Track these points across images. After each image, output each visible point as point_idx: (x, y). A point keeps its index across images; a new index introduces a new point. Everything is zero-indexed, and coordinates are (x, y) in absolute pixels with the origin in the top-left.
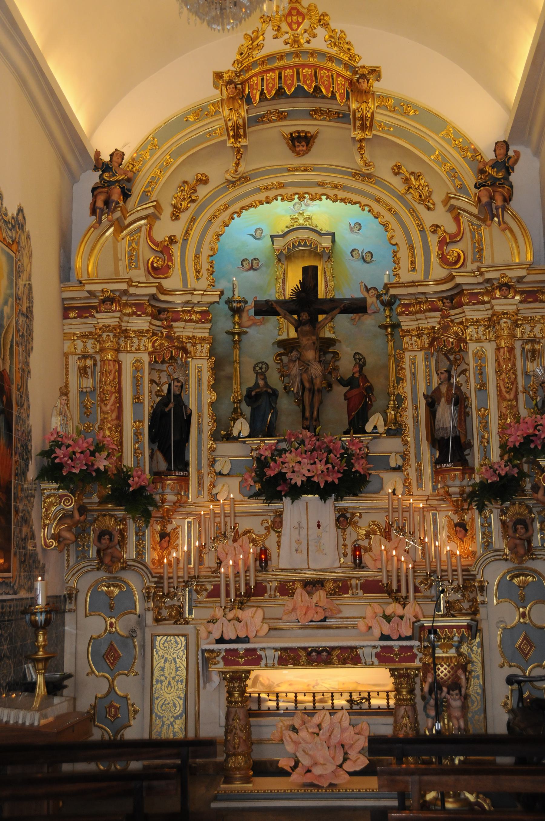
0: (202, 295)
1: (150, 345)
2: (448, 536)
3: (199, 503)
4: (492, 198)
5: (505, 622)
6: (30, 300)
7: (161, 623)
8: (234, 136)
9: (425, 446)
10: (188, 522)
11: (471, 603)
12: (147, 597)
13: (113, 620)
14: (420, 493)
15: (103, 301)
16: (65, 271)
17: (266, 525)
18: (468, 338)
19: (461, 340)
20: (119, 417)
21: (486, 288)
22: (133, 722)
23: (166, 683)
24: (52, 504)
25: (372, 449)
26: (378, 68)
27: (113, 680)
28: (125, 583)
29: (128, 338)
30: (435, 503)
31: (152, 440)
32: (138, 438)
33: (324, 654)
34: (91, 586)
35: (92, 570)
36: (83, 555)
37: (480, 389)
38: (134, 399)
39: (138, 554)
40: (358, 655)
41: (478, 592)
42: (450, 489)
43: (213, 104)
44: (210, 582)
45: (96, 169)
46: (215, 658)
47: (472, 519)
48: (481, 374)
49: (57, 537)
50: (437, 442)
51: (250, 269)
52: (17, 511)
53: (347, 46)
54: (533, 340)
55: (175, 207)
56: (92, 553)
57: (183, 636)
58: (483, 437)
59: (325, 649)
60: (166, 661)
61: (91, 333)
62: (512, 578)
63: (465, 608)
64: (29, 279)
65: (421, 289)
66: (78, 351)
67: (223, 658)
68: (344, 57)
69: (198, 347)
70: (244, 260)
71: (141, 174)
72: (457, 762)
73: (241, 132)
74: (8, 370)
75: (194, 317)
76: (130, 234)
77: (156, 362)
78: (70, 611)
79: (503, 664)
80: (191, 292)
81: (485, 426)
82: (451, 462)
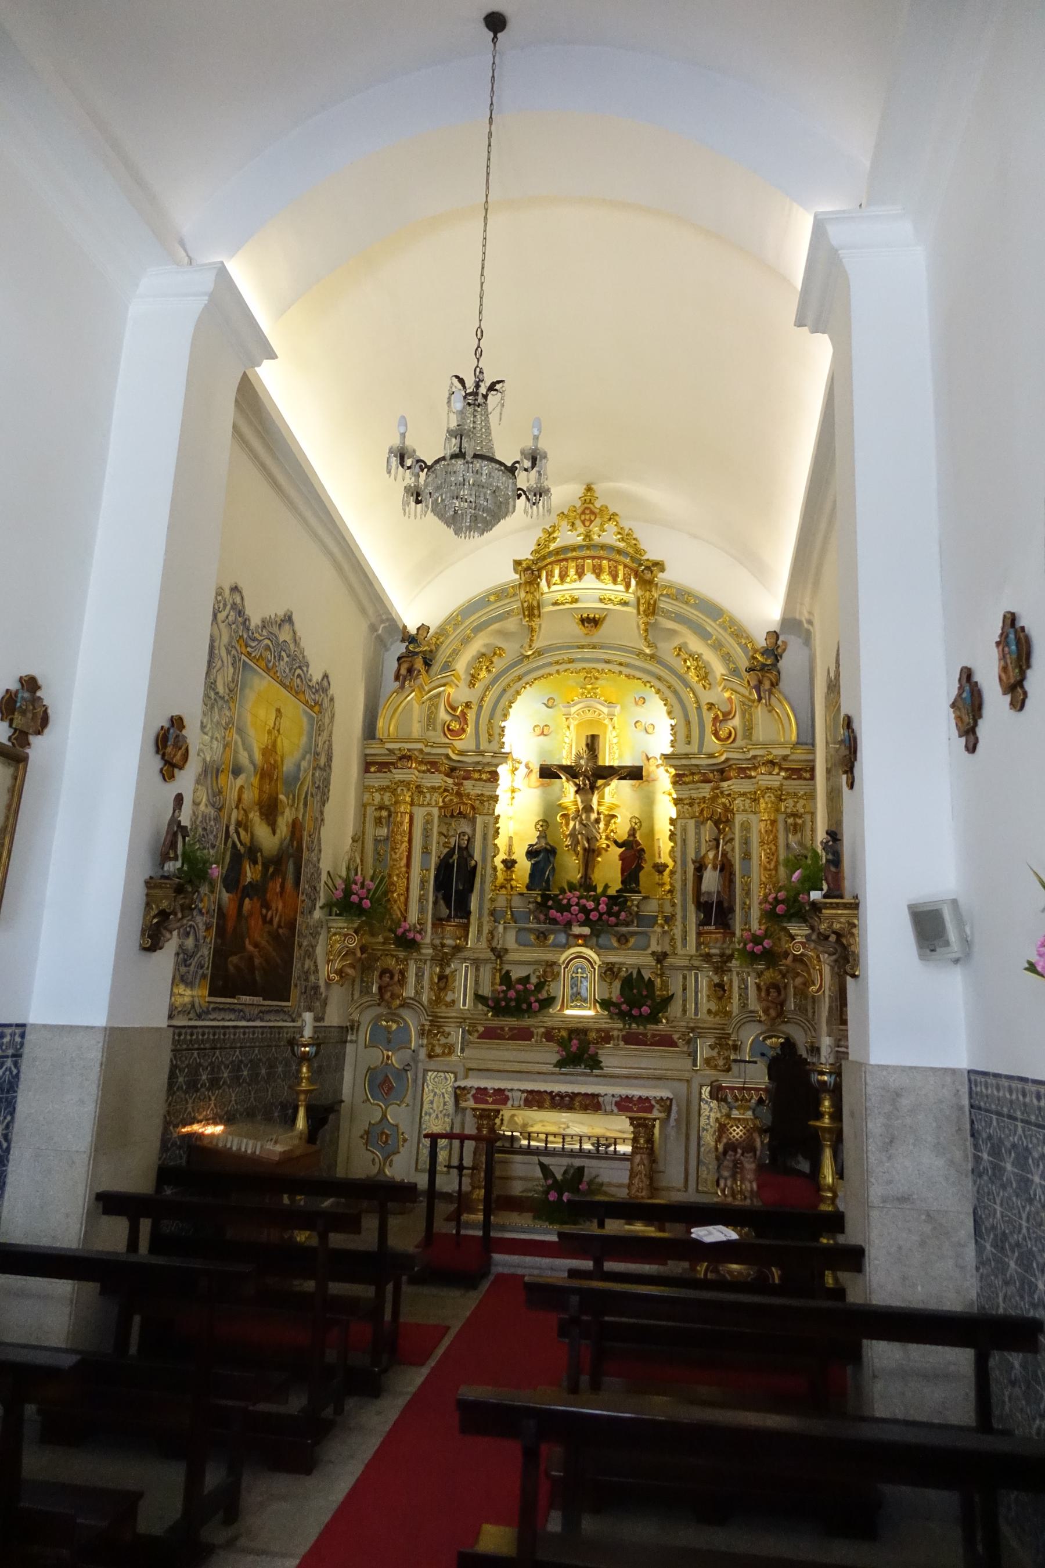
4: (760, 682)
6: (330, 759)
8: (529, 616)
9: (691, 908)
12: (422, 1033)
13: (390, 1053)
15: (400, 759)
16: (370, 732)
19: (727, 809)
20: (408, 865)
22: (401, 1149)
23: (434, 1115)
24: (336, 941)
25: (642, 908)
27: (387, 1108)
28: (404, 1020)
29: (421, 792)
31: (437, 888)
36: (366, 991)
37: (744, 858)
39: (417, 992)
40: (598, 1102)
43: (513, 587)
45: (403, 641)
47: (731, 981)
48: (746, 843)
49: (340, 972)
50: (703, 906)
52: (300, 946)
54: (795, 815)
55: (473, 676)
56: (375, 989)
58: (745, 903)
59: (567, 1095)
60: (435, 1094)
61: (388, 787)
64: (330, 736)
65: (694, 762)
66: (376, 802)
67: (473, 1096)
68: (630, 550)
69: (486, 804)
71: (444, 646)
72: (565, 1199)
73: (536, 612)
74: (300, 817)
75: (484, 776)
76: (430, 699)
78: (351, 1042)
80: (481, 753)
81: (748, 893)
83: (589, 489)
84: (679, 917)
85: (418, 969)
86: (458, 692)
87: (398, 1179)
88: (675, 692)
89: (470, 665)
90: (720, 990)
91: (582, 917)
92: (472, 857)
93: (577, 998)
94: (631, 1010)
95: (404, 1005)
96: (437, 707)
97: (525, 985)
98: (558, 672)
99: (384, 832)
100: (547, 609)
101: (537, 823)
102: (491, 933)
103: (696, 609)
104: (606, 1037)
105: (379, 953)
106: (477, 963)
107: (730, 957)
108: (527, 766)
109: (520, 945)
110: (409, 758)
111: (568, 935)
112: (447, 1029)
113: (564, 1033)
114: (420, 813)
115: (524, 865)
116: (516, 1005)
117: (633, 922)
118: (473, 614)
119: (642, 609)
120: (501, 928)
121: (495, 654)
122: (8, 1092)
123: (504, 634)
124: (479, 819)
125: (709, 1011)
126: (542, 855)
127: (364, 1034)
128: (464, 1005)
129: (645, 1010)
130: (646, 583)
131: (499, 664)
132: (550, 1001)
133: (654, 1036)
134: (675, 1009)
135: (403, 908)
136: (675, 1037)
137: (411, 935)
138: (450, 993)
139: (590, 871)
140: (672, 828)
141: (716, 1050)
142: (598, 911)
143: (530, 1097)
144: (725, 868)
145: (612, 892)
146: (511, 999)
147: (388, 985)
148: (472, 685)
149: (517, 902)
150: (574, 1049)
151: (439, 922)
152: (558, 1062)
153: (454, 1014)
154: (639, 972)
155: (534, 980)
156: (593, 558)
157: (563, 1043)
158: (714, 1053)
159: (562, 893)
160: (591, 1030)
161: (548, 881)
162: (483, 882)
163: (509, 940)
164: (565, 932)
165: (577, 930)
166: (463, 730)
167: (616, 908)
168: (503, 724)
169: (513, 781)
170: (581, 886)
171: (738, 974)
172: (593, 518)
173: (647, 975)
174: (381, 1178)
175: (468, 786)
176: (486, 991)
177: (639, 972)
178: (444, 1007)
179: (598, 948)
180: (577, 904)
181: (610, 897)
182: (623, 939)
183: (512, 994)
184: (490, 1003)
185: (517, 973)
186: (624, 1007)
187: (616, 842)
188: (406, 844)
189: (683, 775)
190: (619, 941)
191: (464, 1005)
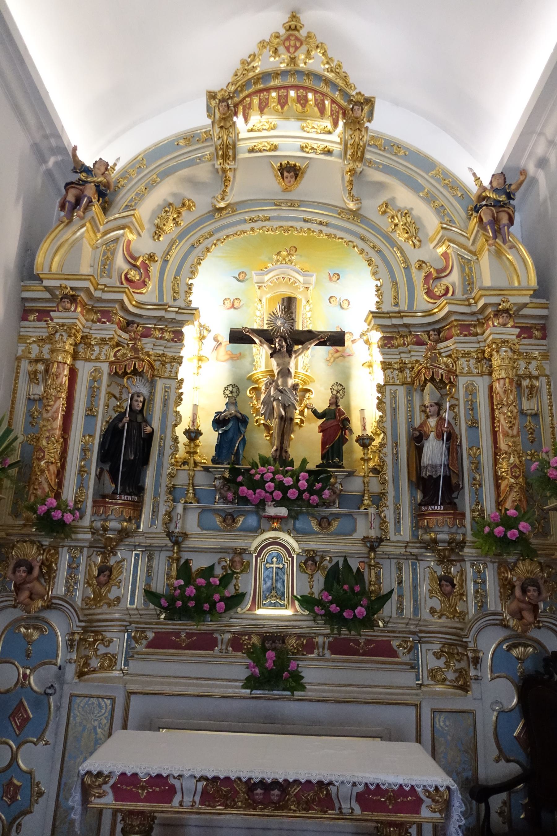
0: (177, 312)
1: (112, 354)
2: (430, 590)
3: (151, 533)
5: (501, 703)
7: (86, 677)
11: (457, 675)
12: (70, 645)
17: (224, 564)
18: (458, 371)
21: (478, 320)
26: (374, 98)
27: (18, 748)
29: (89, 345)
30: (415, 551)
32: (86, 455)
37: (471, 427)
38: (86, 411)
39: (68, 590)
40: (329, 794)
41: (471, 665)
42: (438, 536)
46: (100, 786)
47: (462, 573)
48: (472, 409)
51: (231, 308)
53: (344, 74)
55: (158, 227)
58: (474, 479)
63: (449, 678)
65: (407, 321)
67: (113, 787)
68: (341, 84)
69: (168, 366)
70: (225, 299)
77: (116, 373)
79: (499, 757)
80: (163, 306)
82: (441, 504)
83: (294, 17)
84: (390, 496)
85: (73, 559)
86: (143, 245)
88: (379, 252)
89: (155, 214)
90: (446, 585)
91: (278, 494)
92: (147, 422)
93: (276, 595)
94: (342, 611)
95: (50, 606)
96: (113, 253)
97: (207, 579)
98: (253, 229)
99: (39, 390)
100: (243, 155)
101: (226, 389)
102: (169, 514)
103: (406, 160)
104: (309, 646)
105: (15, 539)
106: (150, 551)
107: (462, 544)
108: (216, 339)
109: (203, 529)
110: (73, 299)
111: (260, 518)
112: (108, 635)
113: (255, 640)
114: (85, 370)
115: (210, 438)
116: (196, 604)
117: (334, 502)
118: (159, 160)
119: (349, 152)
120: (180, 508)
121: (184, 205)
123: (193, 182)
124: (160, 384)
125: (433, 611)
126: (231, 425)
128: (132, 603)
129: (361, 611)
130: (355, 124)
131: (187, 218)
133: (368, 642)
134: (390, 609)
135: (53, 481)
136: (395, 643)
137: (58, 515)
138: (114, 588)
139: (286, 443)
140: (379, 395)
141: (443, 660)
142: (298, 488)
144: (450, 438)
145: (311, 466)
146: (190, 598)
147: (25, 582)
148: (158, 232)
149: (201, 478)
150: (269, 664)
151: (101, 499)
152: (248, 679)
153: (117, 616)
154: (345, 561)
155: (219, 571)
156: (296, 87)
157: (256, 655)
158: (441, 663)
159: (249, 472)
160: (290, 635)
161: (237, 454)
162: (161, 453)
163: (191, 523)
164: (257, 513)
165: (272, 511)
166: (144, 284)
167: (318, 485)
168: (190, 281)
169: (200, 349)
170: (275, 459)
171: (473, 565)
172: (298, 45)
173: (354, 564)
175: (148, 341)
177: (345, 561)
178: (105, 607)
179: (297, 533)
180: (272, 480)
181: (310, 472)
183: (191, 591)
185: (199, 563)
186: (334, 608)
187: (315, 412)
188: (62, 402)
189: (392, 338)
190: (320, 525)
191: (132, 603)
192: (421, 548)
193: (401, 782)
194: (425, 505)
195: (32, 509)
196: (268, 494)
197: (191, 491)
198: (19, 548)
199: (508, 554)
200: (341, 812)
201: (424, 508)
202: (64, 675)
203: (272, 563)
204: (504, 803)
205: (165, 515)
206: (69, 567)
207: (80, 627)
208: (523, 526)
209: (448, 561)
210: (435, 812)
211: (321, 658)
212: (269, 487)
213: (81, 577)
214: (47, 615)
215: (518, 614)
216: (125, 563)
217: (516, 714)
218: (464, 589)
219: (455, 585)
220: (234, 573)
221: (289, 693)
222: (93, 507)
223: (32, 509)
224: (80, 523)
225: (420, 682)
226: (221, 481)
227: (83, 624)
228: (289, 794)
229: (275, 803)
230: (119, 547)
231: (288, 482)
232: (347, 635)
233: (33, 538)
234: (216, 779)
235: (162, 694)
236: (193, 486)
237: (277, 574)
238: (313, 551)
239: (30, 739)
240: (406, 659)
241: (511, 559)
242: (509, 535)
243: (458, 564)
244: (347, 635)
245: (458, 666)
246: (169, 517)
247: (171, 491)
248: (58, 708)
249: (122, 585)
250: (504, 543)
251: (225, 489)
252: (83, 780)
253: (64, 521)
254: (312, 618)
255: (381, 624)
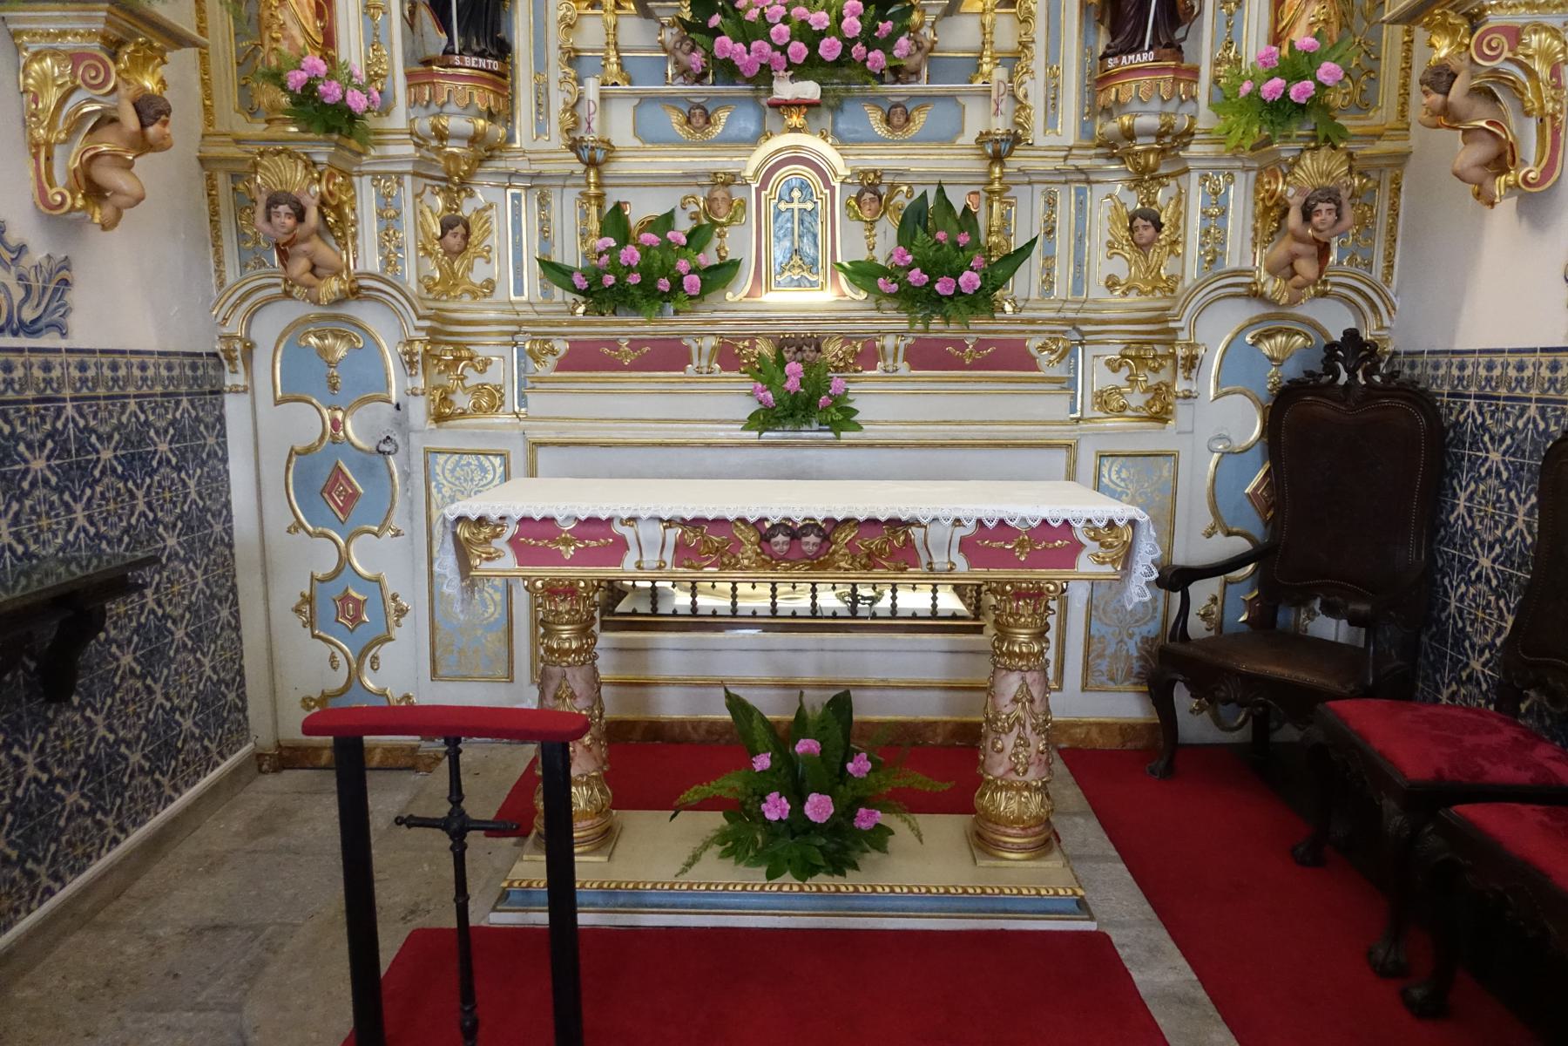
10: (514, 196)
12: (409, 363)
14: (1051, 140)
22: (396, 632)
24: (44, 80)
27: (348, 543)
28: (365, 331)
33: (812, 539)
34: (283, 335)
35: (269, 301)
39: (387, 261)
40: (909, 541)
41: (1180, 371)
42: (1137, 120)
44: (563, 334)
46: (487, 541)
47: (1180, 198)
57: (496, 455)
62: (1258, 339)
67: (513, 541)
78: (235, 390)
84: (1039, 50)
85: (385, 200)
87: (395, 694)
90: (1145, 227)
91: (799, 50)
93: (804, 264)
94: (931, 283)
95: (355, 293)
104: (868, 356)
106: (538, 183)
107: (1187, 136)
113: (765, 348)
122: (139, 445)
125: (1112, 283)
127: (268, 371)
128: (519, 290)
129: (970, 280)
132: (723, 273)
134: (1025, 282)
136: (1033, 344)
138: (479, 264)
141: (1125, 372)
143: (692, 539)
146: (630, 269)
150: (792, 384)
151: (422, 70)
153: (492, 315)
154: (941, 191)
157: (764, 372)
158: (1120, 379)
163: (620, 126)
165: (786, 89)
167: (886, 27)
171: (1205, 178)
173: (958, 199)
174: (353, 700)
176: (570, 254)
177: (941, 191)
178: (467, 298)
179: (842, 141)
180: (785, 20)
182: (898, 117)
184: (578, 280)
186: (916, 276)
190: (888, 121)
191: (519, 290)
192: (1097, 156)
193: (1045, 515)
194: (1113, 55)
195: (276, 78)
196: (777, 54)
197: (613, 59)
198: (267, 168)
199: (1287, 138)
200: (931, 569)
201: (1111, 62)
202: (407, 419)
203: (792, 200)
204: (1214, 600)
205: (565, 111)
206: (380, 215)
207: (422, 329)
208: (1328, 71)
209: (1152, 178)
210: (1104, 563)
211: (890, 376)
212: (780, 35)
213: (407, 234)
214: (354, 310)
215: (1286, 269)
216: (492, 212)
217: (1256, 454)
218: (1181, 231)
219: (1162, 225)
220: (715, 224)
221: (831, 435)
222: (409, 86)
223: (276, 78)
224: (387, 124)
225: (1078, 415)
226: (676, 30)
227: (427, 323)
228: (836, 543)
229: (808, 558)
230: (477, 180)
231: (819, 23)
232: (941, 331)
233: (291, 147)
234: (698, 522)
235: (594, 444)
236: (618, 52)
237: (801, 222)
238: (875, 172)
239: (367, 527)
240: (1058, 371)
241: (1287, 151)
242: (1292, 96)
243: (1172, 183)
244: (941, 331)
245: (1153, 380)
246: (573, 115)
247: (569, 59)
248: (407, 475)
249: (494, 256)
250: (1281, 111)
251: (686, 48)
252: (455, 535)
253: (349, 108)
254: (873, 306)
255: (1008, 308)
